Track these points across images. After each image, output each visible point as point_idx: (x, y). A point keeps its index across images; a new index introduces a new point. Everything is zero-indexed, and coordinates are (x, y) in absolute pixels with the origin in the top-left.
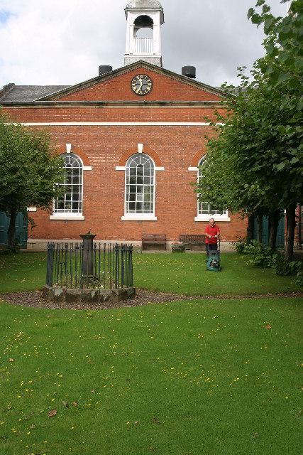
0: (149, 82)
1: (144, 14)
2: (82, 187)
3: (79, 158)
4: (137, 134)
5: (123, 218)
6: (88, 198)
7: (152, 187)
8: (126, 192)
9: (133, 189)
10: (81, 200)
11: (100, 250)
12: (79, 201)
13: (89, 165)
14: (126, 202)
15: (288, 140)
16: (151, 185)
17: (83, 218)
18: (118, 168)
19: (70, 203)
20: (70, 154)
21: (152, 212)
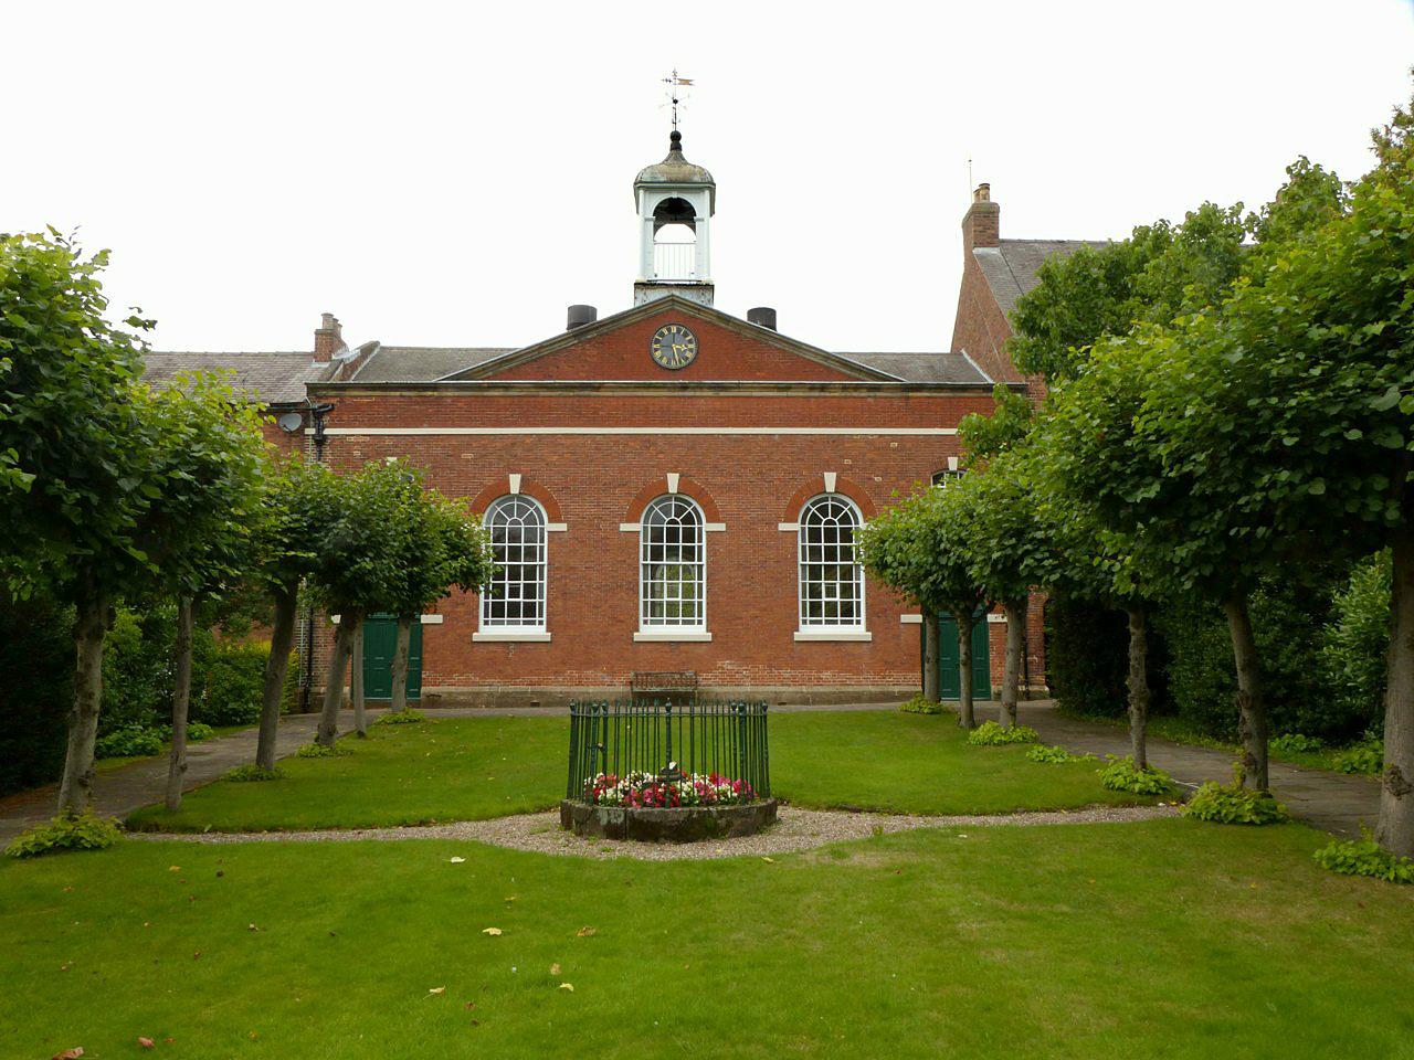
0: (669, 330)
1: (675, 195)
2: (546, 569)
3: (695, 504)
4: (687, 455)
5: (637, 637)
6: (559, 592)
7: (700, 567)
8: (803, 581)
9: (815, 572)
10: (542, 600)
11: (723, 716)
12: (537, 600)
13: (719, 521)
14: (804, 600)
15: (1149, 435)
16: (538, 563)
17: (547, 636)
18: (624, 527)
19: (661, 604)
20: (518, 496)
21: (700, 622)
